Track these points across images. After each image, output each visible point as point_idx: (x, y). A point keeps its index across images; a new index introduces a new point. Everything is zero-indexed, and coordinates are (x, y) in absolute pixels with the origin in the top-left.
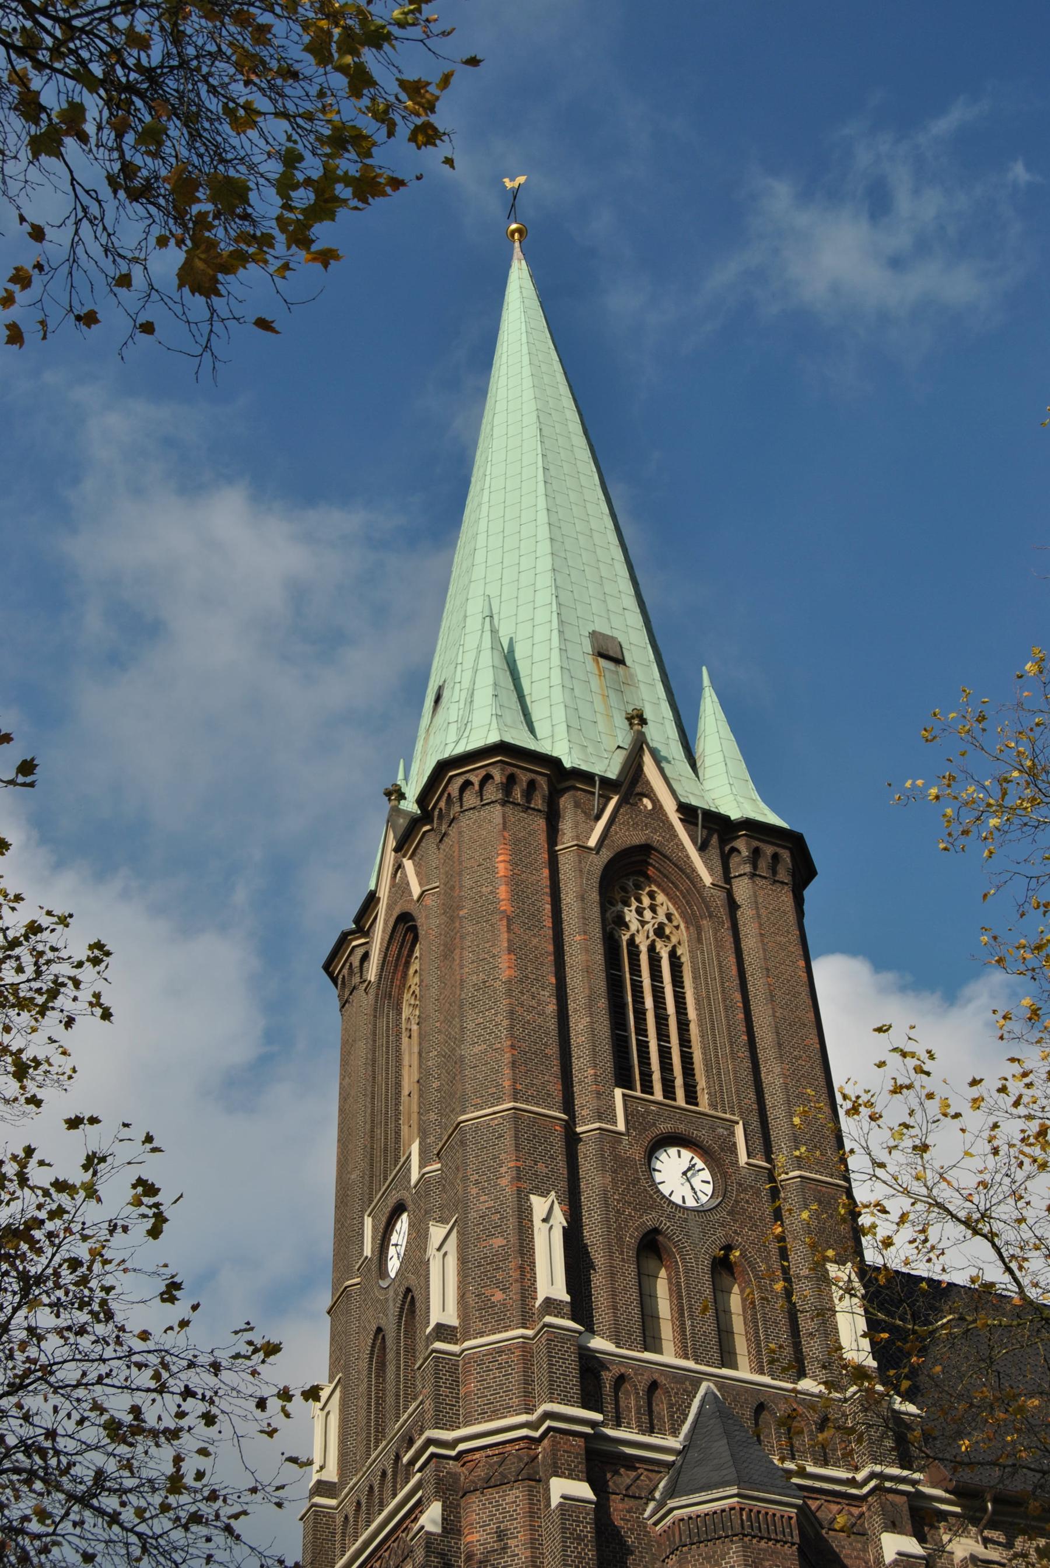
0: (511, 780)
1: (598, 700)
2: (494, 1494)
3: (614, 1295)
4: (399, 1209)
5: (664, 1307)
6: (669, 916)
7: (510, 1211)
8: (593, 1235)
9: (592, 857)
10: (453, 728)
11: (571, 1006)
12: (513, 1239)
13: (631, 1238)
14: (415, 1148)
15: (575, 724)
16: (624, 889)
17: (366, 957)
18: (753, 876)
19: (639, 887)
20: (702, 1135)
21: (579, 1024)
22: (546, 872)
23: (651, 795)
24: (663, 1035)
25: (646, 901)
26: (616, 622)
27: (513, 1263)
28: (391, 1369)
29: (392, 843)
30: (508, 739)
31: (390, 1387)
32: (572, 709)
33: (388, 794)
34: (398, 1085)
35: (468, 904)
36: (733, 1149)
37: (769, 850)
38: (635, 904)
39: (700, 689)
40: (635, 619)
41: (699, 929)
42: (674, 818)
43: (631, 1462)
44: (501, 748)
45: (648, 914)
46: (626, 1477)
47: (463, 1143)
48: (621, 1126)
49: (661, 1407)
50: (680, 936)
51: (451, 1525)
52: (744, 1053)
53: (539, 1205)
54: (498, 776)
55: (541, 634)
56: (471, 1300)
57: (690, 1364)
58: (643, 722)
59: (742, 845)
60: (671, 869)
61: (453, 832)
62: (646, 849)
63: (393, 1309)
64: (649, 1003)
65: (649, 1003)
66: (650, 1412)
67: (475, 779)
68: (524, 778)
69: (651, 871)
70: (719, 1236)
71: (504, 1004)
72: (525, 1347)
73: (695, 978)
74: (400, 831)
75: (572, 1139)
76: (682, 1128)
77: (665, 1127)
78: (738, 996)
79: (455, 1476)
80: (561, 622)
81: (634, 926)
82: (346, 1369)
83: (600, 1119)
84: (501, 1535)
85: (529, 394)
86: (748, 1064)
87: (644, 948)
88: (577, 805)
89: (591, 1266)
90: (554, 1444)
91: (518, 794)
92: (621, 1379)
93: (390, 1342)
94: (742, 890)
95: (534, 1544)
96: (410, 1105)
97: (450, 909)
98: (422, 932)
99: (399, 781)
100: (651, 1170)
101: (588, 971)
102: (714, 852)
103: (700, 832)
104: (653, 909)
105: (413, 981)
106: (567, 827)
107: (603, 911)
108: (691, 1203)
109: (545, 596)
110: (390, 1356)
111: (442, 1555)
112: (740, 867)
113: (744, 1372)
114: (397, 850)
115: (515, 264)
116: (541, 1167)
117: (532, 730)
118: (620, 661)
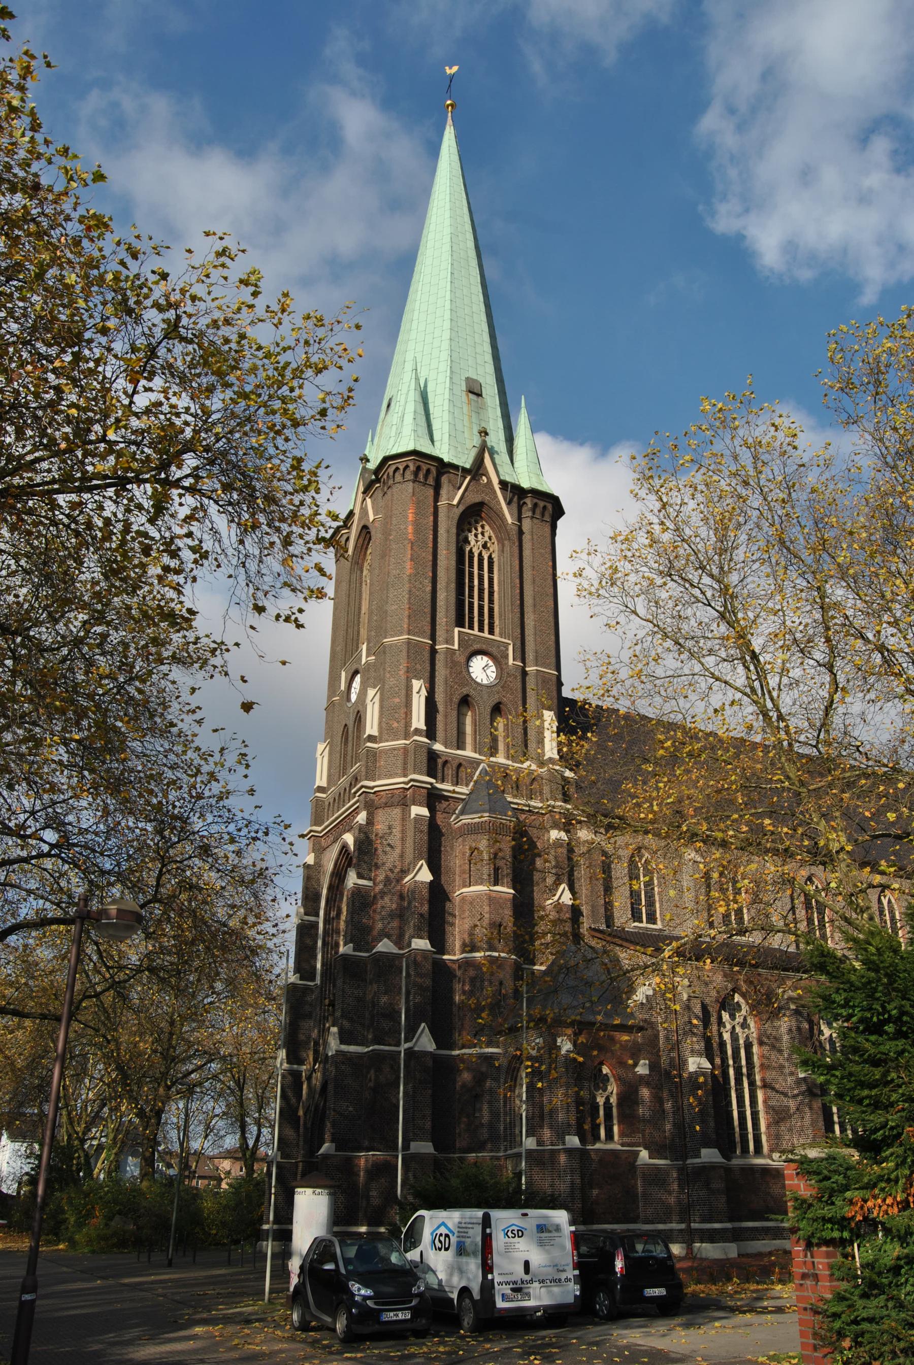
0: (418, 468)
1: (466, 418)
2: (388, 810)
3: (446, 725)
4: (356, 672)
5: (469, 729)
6: (490, 538)
7: (403, 687)
8: (439, 697)
9: (455, 509)
10: (394, 428)
11: (439, 586)
12: (404, 700)
13: (456, 699)
14: (364, 647)
15: (453, 434)
16: (470, 524)
17: (348, 539)
18: (532, 518)
19: (477, 522)
20: (494, 650)
21: (441, 596)
22: (431, 518)
23: (486, 474)
24: (481, 598)
25: (480, 529)
26: (481, 371)
27: (403, 710)
28: (350, 744)
29: (362, 489)
30: (419, 448)
31: (350, 753)
32: (453, 425)
33: (361, 459)
34: (360, 609)
35: (394, 533)
36: (507, 657)
37: (541, 504)
38: (474, 531)
39: (520, 408)
40: (490, 368)
41: (503, 546)
42: (497, 487)
43: (447, 798)
44: (415, 453)
45: (480, 536)
46: (444, 804)
47: (384, 653)
48: (456, 647)
49: (462, 774)
50: (494, 547)
51: (370, 822)
52: (517, 610)
53: (417, 684)
54: (412, 467)
55: (441, 378)
56: (384, 725)
57: (477, 756)
58: (486, 434)
59: (529, 501)
60: (493, 514)
61: (389, 492)
62: (481, 504)
63: (352, 717)
64: (476, 582)
65: (476, 582)
66: (457, 776)
67: (401, 467)
68: (425, 467)
69: (483, 515)
70: (495, 699)
71: (407, 587)
72: (405, 749)
73: (499, 570)
74: (367, 482)
75: (433, 652)
76: (484, 647)
77: (476, 647)
78: (518, 581)
79: (373, 801)
80: (452, 372)
81: (473, 543)
82: (332, 737)
83: (447, 643)
84: (390, 827)
85: (447, 222)
86: (518, 615)
87: (476, 555)
88: (450, 481)
89: (437, 711)
90: (414, 792)
91: (421, 476)
92: (446, 762)
93: (350, 730)
94: (527, 525)
95: (403, 832)
96: (364, 618)
97: (386, 533)
98: (373, 533)
99: (367, 453)
100: (468, 666)
101: (448, 569)
102: (514, 505)
103: (509, 495)
104: (483, 534)
105: (369, 557)
106: (444, 492)
107: (458, 535)
108: (485, 682)
109: (445, 355)
110: (350, 739)
111: (365, 833)
112: (527, 513)
113: (501, 759)
114: (364, 493)
115: (448, 127)
116: (418, 666)
117: (432, 441)
118: (479, 395)
